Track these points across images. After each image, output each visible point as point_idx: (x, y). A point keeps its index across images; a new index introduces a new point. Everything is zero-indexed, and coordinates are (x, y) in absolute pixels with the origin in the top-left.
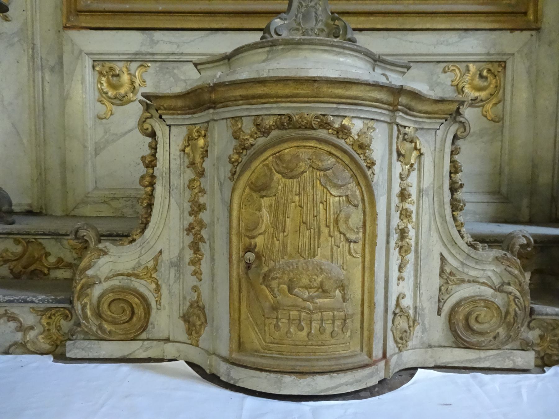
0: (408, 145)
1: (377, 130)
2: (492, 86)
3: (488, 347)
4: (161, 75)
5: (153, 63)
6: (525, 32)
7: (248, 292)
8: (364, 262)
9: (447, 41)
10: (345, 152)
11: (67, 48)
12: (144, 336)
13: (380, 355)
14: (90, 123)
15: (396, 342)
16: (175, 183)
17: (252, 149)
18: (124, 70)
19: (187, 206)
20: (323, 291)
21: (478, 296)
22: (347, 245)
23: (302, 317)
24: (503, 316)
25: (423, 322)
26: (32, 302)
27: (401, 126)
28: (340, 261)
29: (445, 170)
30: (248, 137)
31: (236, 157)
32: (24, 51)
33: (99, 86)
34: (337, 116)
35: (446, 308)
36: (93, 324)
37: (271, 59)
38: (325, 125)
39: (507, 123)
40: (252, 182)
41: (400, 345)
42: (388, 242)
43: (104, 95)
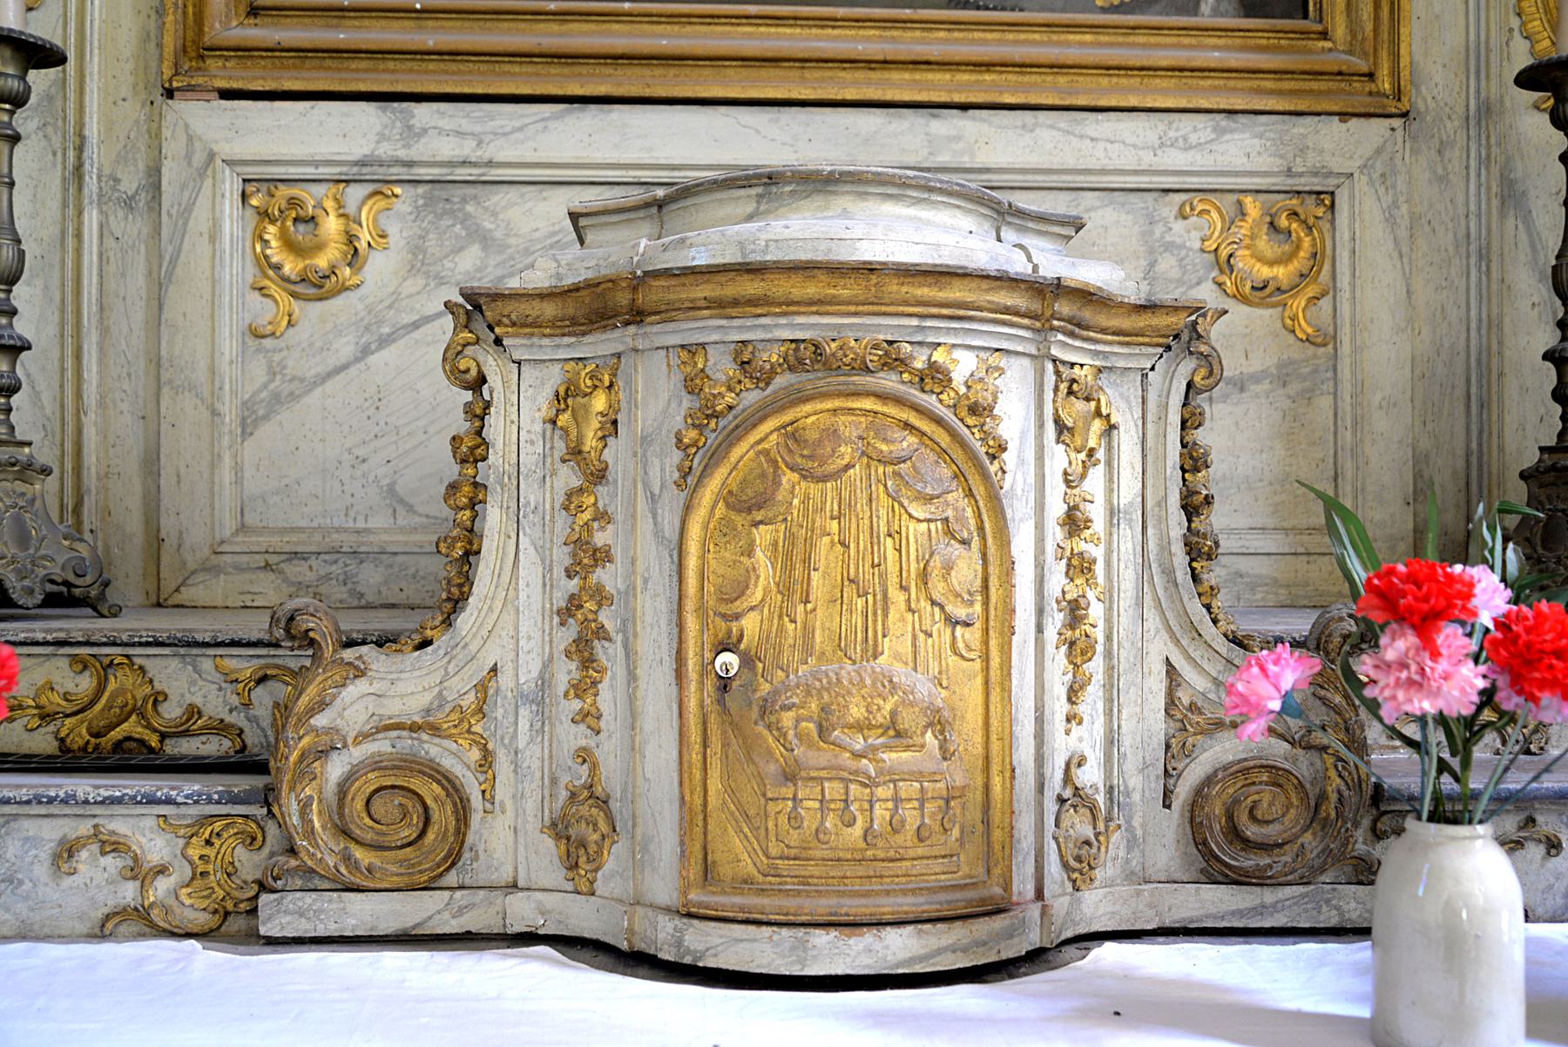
0: (1080, 406)
1: (1009, 373)
2: (1302, 254)
3: (1282, 879)
4: (430, 217)
5: (407, 186)
6: (1375, 123)
7: (726, 745)
8: (986, 669)
9: (1185, 140)
10: (939, 421)
11: (173, 147)
12: (451, 879)
13: (1030, 892)
14: (228, 346)
15: (1065, 865)
16: (532, 499)
17: (730, 417)
18: (329, 204)
19: (562, 557)
20: (897, 733)
21: (1253, 758)
22: (949, 631)
23: (852, 793)
24: (1313, 803)
25: (1128, 822)
26: (169, 801)
27: (1063, 363)
28: (934, 668)
29: (1169, 463)
30: (723, 389)
31: (693, 434)
32: (54, 154)
33: (258, 249)
34: (920, 343)
35: (1183, 790)
36: (325, 850)
37: (768, 212)
38: (894, 361)
39: (1345, 349)
40: (730, 492)
41: (1076, 875)
42: (1040, 629)
43: (271, 273)
